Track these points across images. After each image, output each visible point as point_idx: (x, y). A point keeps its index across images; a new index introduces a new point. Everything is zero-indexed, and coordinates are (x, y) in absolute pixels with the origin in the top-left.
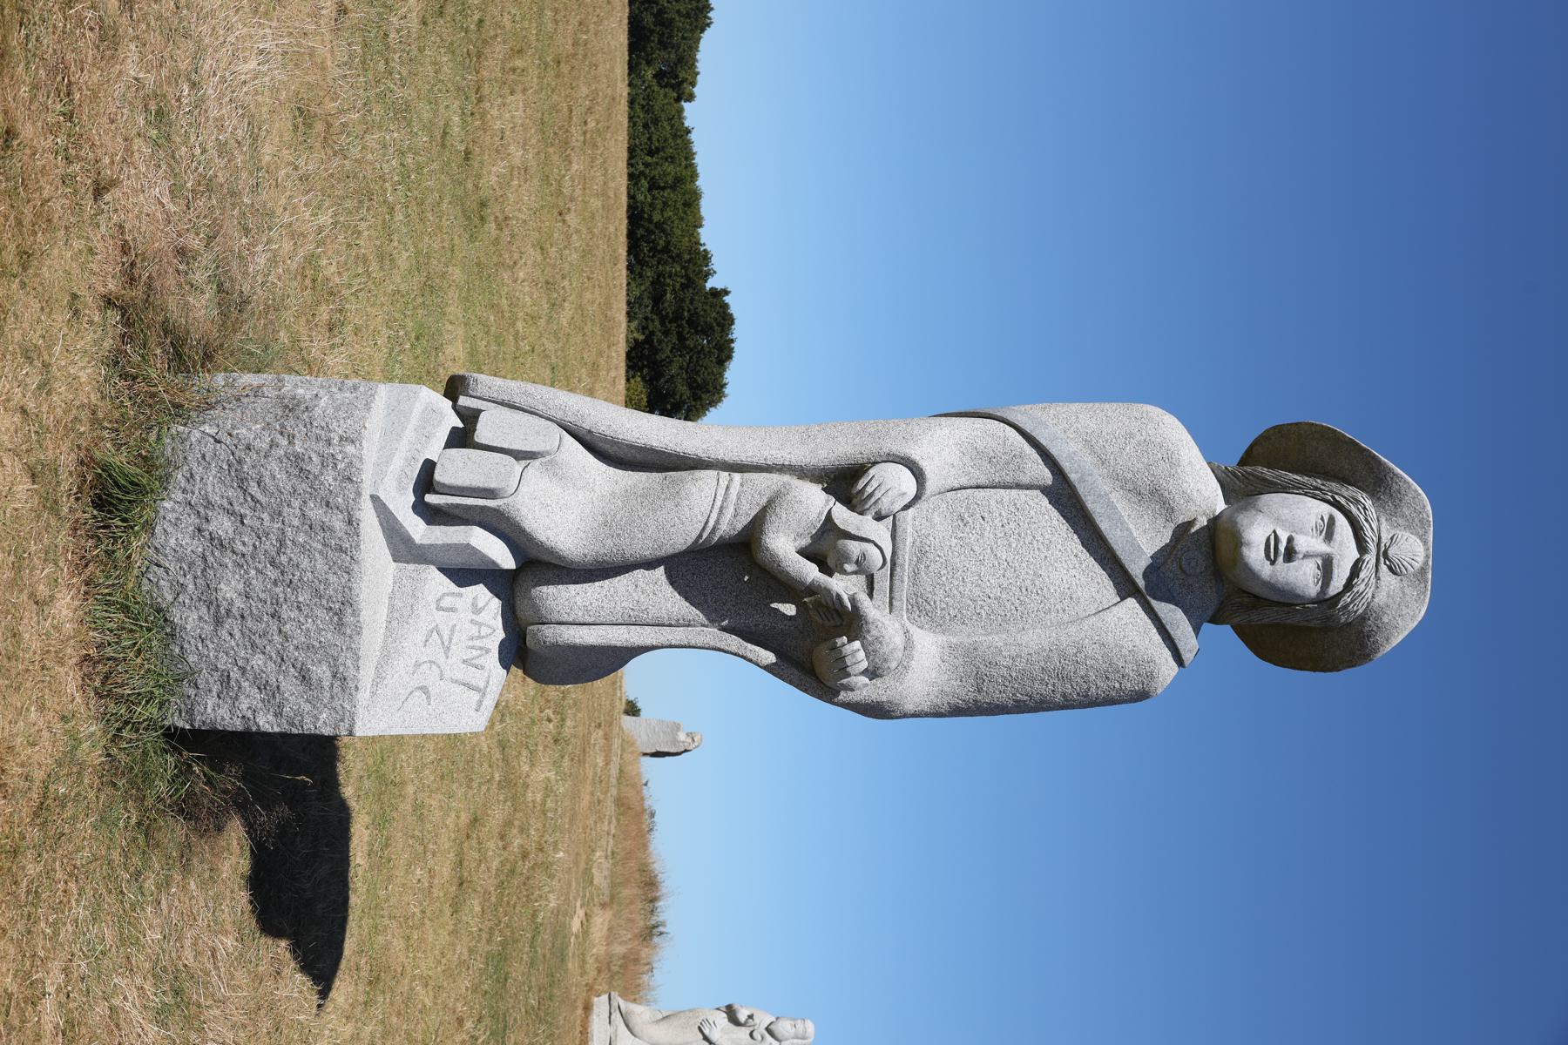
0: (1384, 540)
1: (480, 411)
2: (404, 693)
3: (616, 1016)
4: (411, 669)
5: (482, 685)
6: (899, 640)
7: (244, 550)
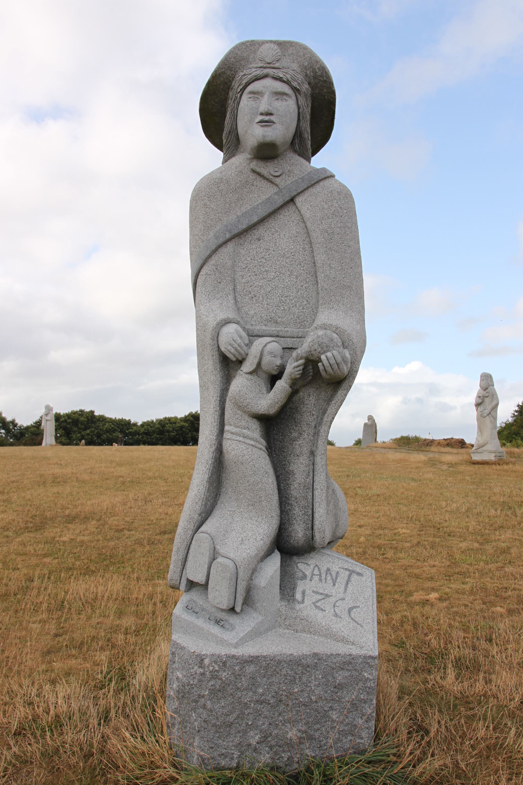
0: (262, 65)
1: (188, 580)
2: (352, 624)
3: (480, 450)
4: (339, 619)
5: (348, 573)
6: (321, 333)
7: (267, 723)
